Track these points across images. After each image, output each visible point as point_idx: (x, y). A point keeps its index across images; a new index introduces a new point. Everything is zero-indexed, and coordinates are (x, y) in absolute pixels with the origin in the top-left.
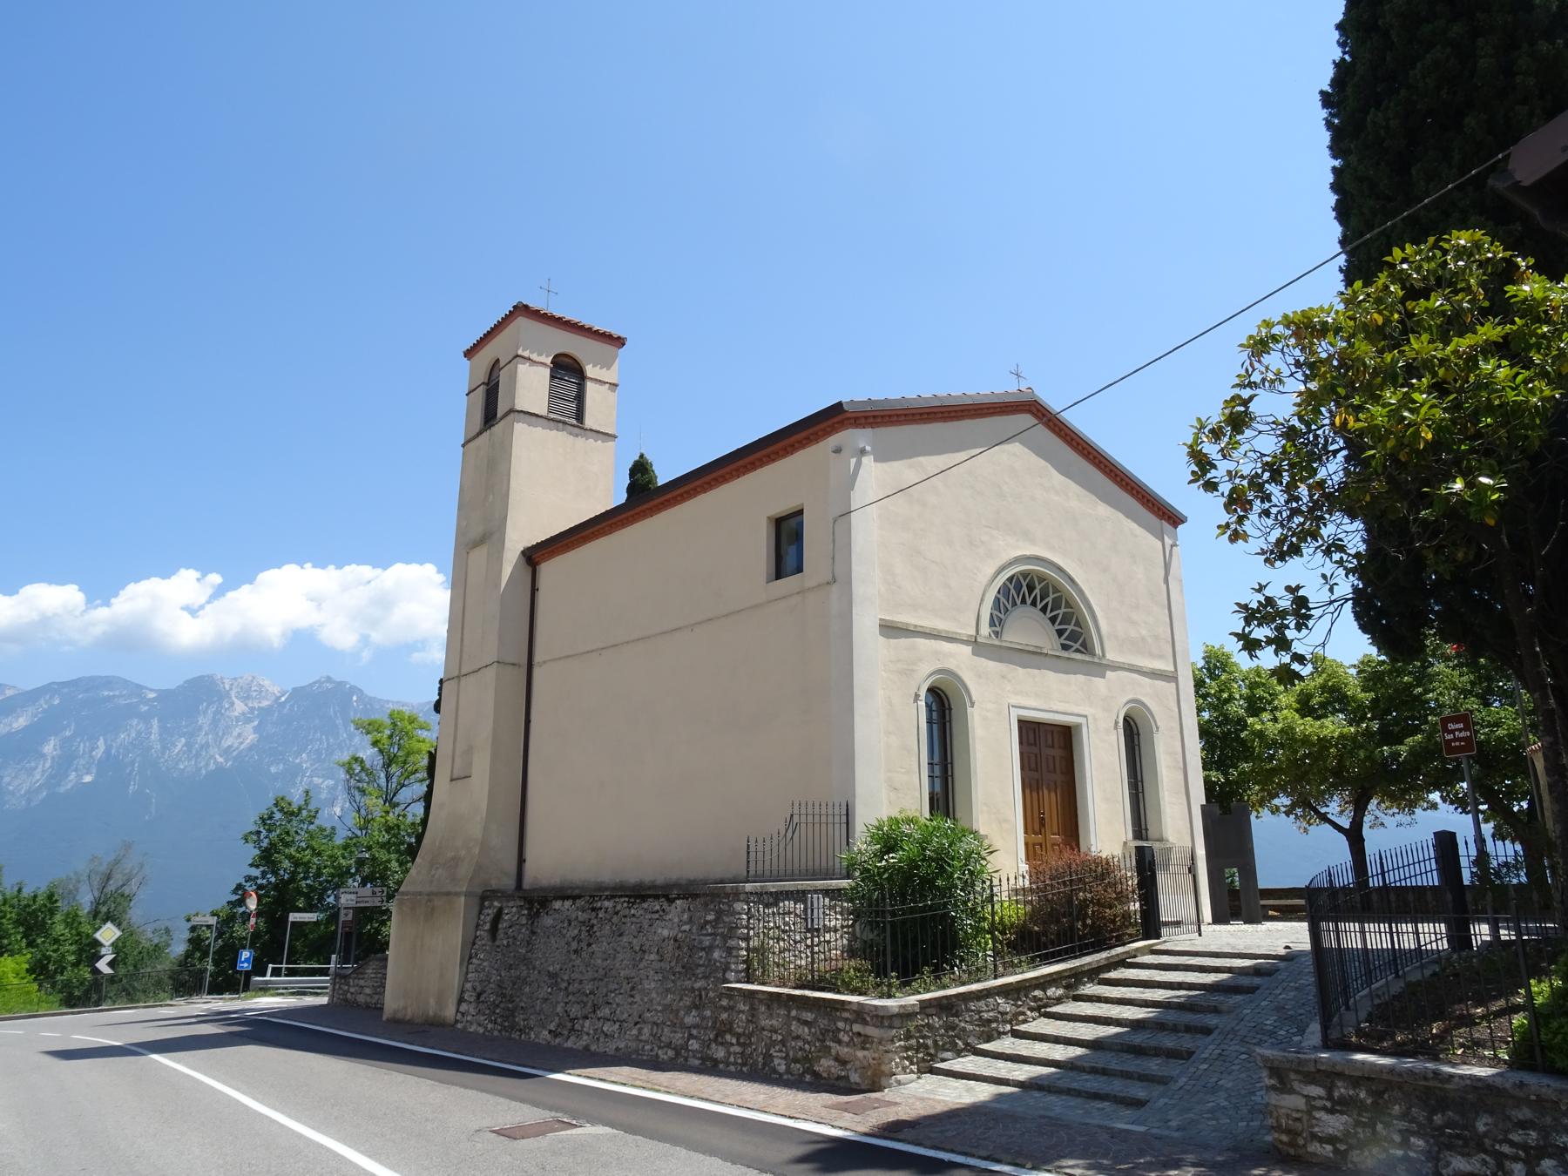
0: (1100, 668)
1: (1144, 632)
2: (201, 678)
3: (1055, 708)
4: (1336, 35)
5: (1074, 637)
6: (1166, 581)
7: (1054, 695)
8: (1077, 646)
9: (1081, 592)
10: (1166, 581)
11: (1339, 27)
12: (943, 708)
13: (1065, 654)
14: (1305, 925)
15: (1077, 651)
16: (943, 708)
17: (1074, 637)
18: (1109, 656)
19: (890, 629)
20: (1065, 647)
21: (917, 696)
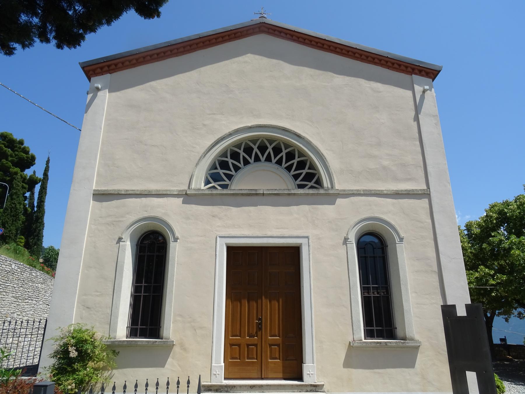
0: (331, 197)
1: (386, 163)
2: (44, 224)
3: (269, 234)
4: (82, 43)
5: (309, 177)
6: (417, 119)
7: (266, 225)
8: (312, 184)
9: (308, 143)
10: (417, 119)
11: (95, 32)
12: (152, 252)
13: (301, 191)
14: (494, 343)
15: (312, 187)
16: (152, 252)
17: (309, 177)
18: (337, 186)
19: (101, 196)
20: (300, 186)
21: (346, 240)
